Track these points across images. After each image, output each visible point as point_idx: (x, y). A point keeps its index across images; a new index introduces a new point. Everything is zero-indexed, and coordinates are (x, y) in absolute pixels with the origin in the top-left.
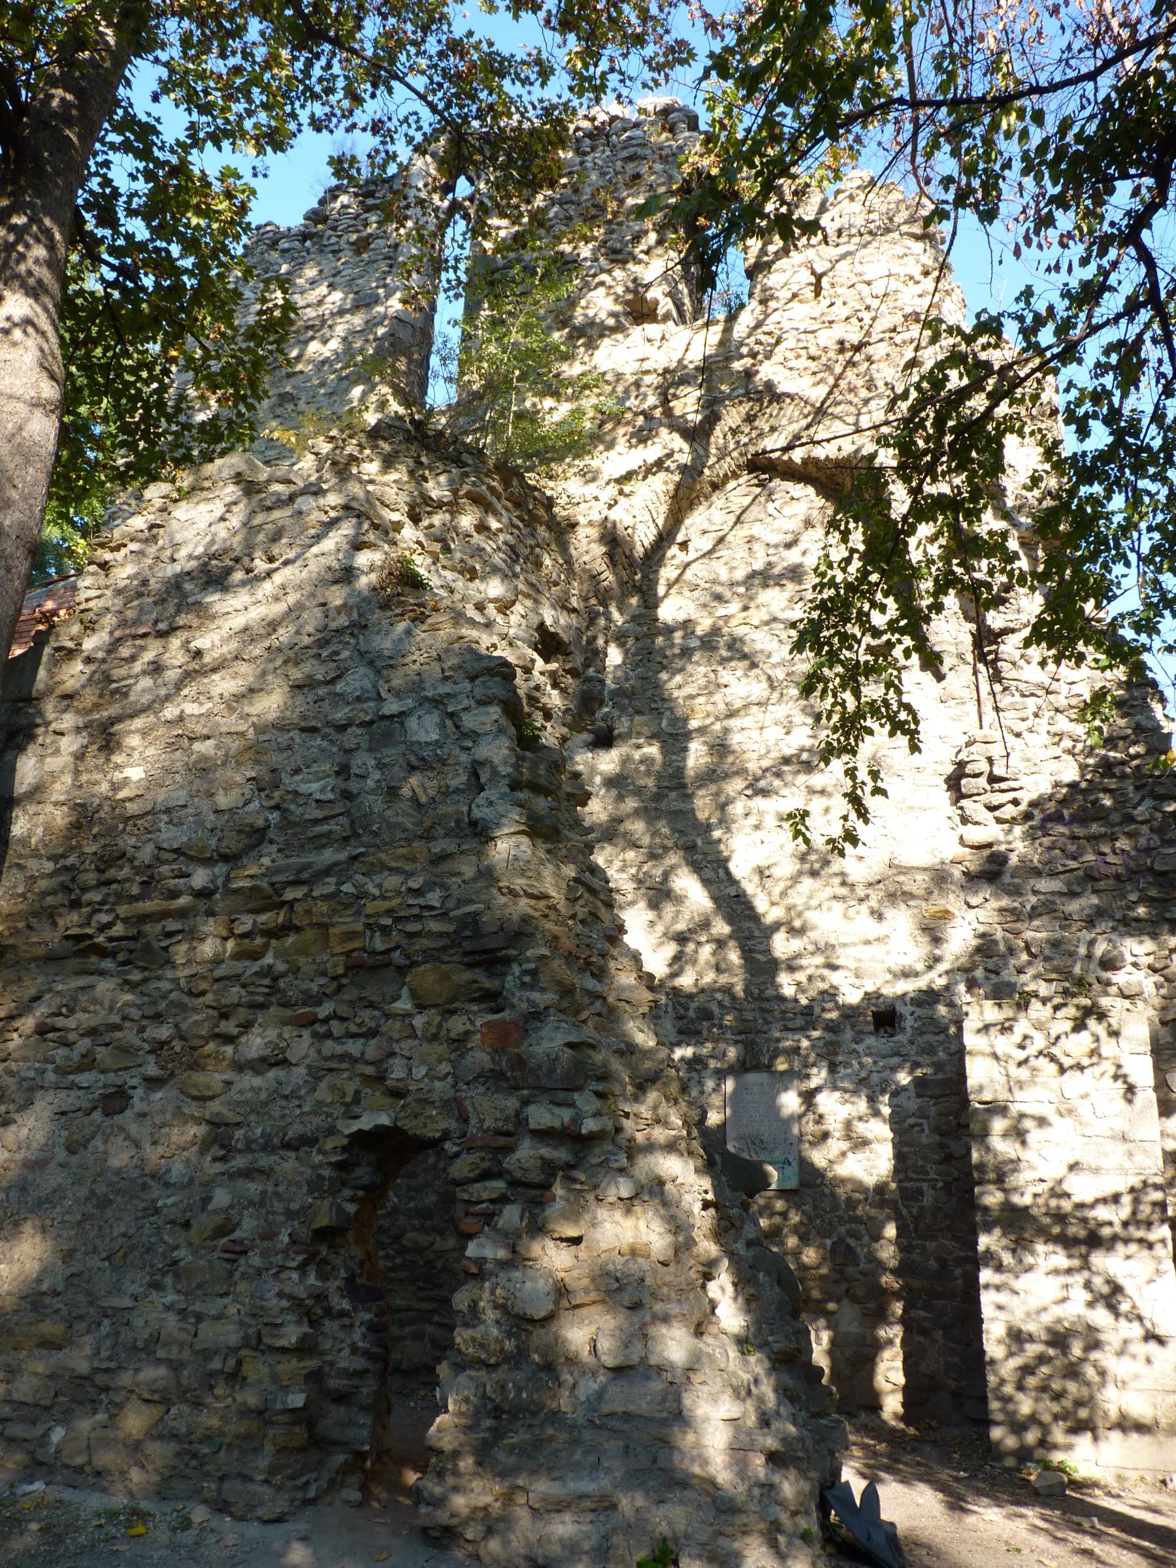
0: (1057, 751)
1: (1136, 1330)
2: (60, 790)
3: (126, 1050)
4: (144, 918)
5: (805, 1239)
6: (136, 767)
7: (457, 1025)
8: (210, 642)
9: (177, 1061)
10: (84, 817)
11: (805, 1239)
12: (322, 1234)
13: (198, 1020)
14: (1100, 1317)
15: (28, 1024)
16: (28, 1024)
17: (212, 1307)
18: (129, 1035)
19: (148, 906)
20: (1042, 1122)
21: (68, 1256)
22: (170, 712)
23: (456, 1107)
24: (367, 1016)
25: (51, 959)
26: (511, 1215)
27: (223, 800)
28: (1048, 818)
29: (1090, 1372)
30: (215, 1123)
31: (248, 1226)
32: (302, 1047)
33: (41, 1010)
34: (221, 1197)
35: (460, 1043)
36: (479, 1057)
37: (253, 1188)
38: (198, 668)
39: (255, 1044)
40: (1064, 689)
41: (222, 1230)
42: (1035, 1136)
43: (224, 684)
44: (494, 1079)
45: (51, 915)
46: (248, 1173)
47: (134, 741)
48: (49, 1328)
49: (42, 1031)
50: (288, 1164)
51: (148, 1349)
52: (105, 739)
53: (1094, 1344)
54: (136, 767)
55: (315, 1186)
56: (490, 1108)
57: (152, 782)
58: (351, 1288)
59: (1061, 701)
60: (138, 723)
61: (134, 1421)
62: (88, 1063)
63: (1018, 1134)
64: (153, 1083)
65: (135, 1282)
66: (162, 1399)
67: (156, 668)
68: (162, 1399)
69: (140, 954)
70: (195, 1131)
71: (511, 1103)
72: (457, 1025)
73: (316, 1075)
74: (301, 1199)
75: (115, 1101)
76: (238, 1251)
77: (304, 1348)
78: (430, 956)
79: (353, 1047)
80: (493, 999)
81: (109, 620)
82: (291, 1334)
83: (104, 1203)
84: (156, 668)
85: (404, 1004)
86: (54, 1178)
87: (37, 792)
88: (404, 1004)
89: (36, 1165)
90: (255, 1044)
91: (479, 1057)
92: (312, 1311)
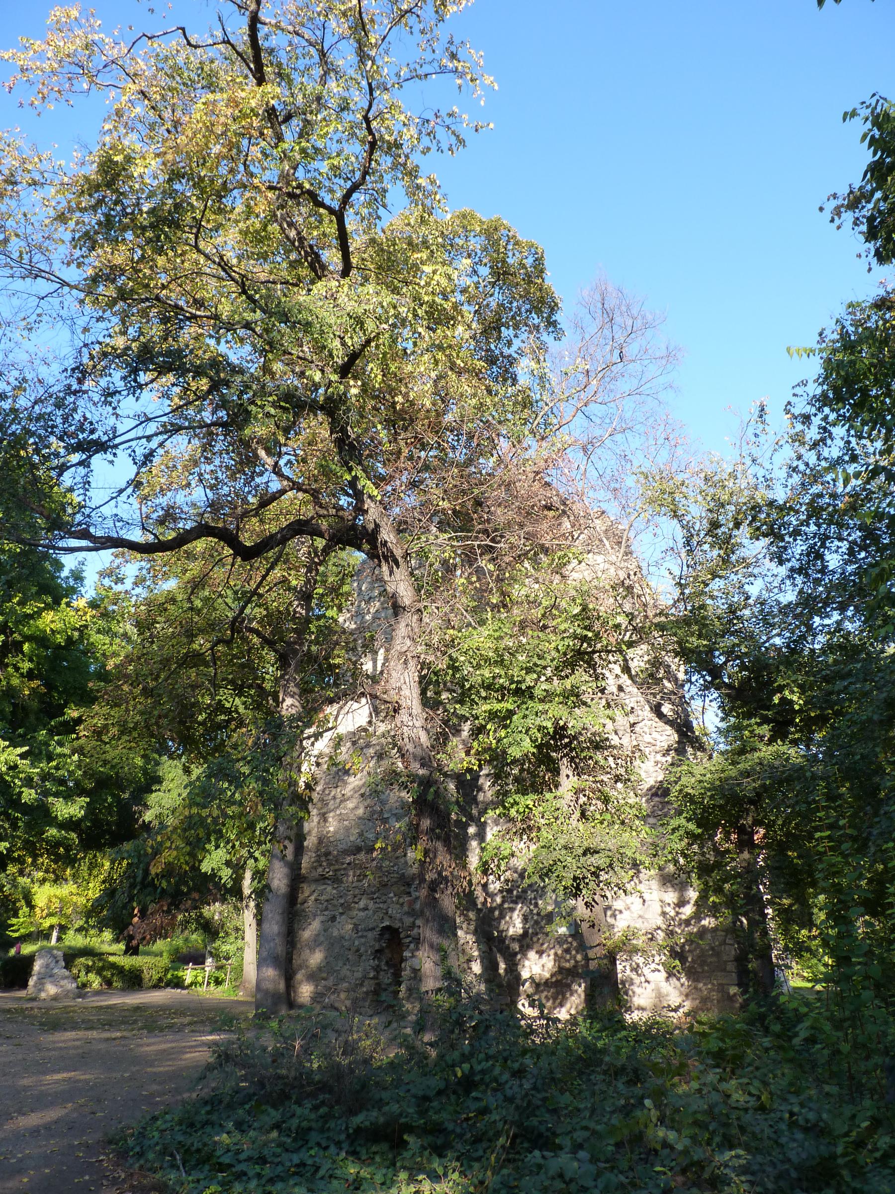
0: (657, 768)
1: (643, 979)
2: (314, 832)
3: (335, 906)
4: (336, 870)
5: (577, 952)
6: (332, 826)
7: (401, 900)
8: (348, 791)
9: (347, 908)
10: (320, 841)
11: (577, 952)
12: (377, 951)
13: (349, 898)
14: (634, 976)
15: (313, 898)
16: (313, 898)
17: (355, 969)
18: (335, 902)
19: (337, 867)
20: (621, 912)
21: (326, 958)
22: (338, 812)
23: (401, 920)
24: (384, 898)
25: (316, 881)
26: (412, 946)
27: (352, 839)
28: (653, 795)
29: (630, 993)
30: (355, 925)
31: (362, 950)
32: (371, 905)
33: (315, 894)
34: (357, 943)
35: (402, 904)
36: (406, 908)
37: (363, 940)
38: (344, 799)
39: (362, 904)
40: (658, 743)
41: (358, 950)
42: (618, 917)
43: (350, 805)
44: (408, 914)
45: (315, 868)
46: (362, 937)
47: (330, 820)
48: (324, 975)
49: (316, 900)
50: (370, 935)
51: (343, 979)
52: (324, 817)
53: (632, 984)
54: (332, 826)
55: (375, 939)
56: (408, 921)
57: (335, 832)
58: (387, 963)
59: (658, 748)
60: (331, 814)
61: (343, 996)
62: (326, 909)
63: (614, 916)
64: (342, 914)
65: (340, 964)
66: (348, 991)
67: (334, 798)
68: (348, 991)
69: (336, 880)
70: (351, 926)
71: (412, 920)
72: (401, 900)
73: (375, 912)
74: (373, 943)
75: (333, 919)
76: (360, 956)
77: (374, 978)
78: (396, 883)
79: (381, 905)
80: (409, 894)
81: (322, 782)
82: (371, 975)
83: (332, 945)
84: (334, 798)
85: (392, 895)
86: (322, 939)
87: (309, 832)
88: (392, 895)
89: (317, 935)
90: (362, 904)
91: (406, 908)
92: (377, 969)
